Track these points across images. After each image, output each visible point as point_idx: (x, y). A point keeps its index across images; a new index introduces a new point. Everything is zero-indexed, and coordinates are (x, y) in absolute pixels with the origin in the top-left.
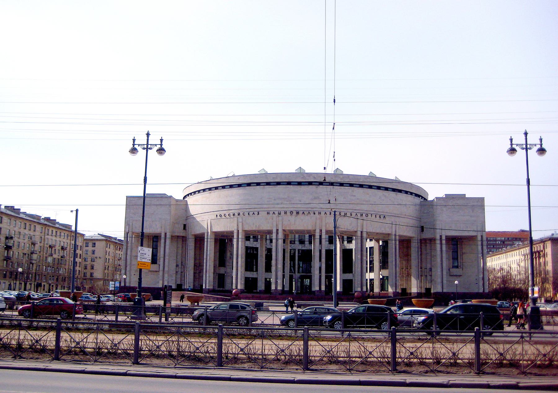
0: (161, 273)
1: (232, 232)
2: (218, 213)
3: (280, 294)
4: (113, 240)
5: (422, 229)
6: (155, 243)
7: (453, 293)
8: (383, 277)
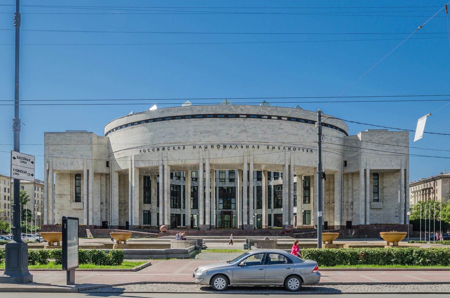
0: (85, 211)
3: (208, 230)
4: (41, 183)
5: (345, 164)
6: (77, 181)
8: (305, 211)
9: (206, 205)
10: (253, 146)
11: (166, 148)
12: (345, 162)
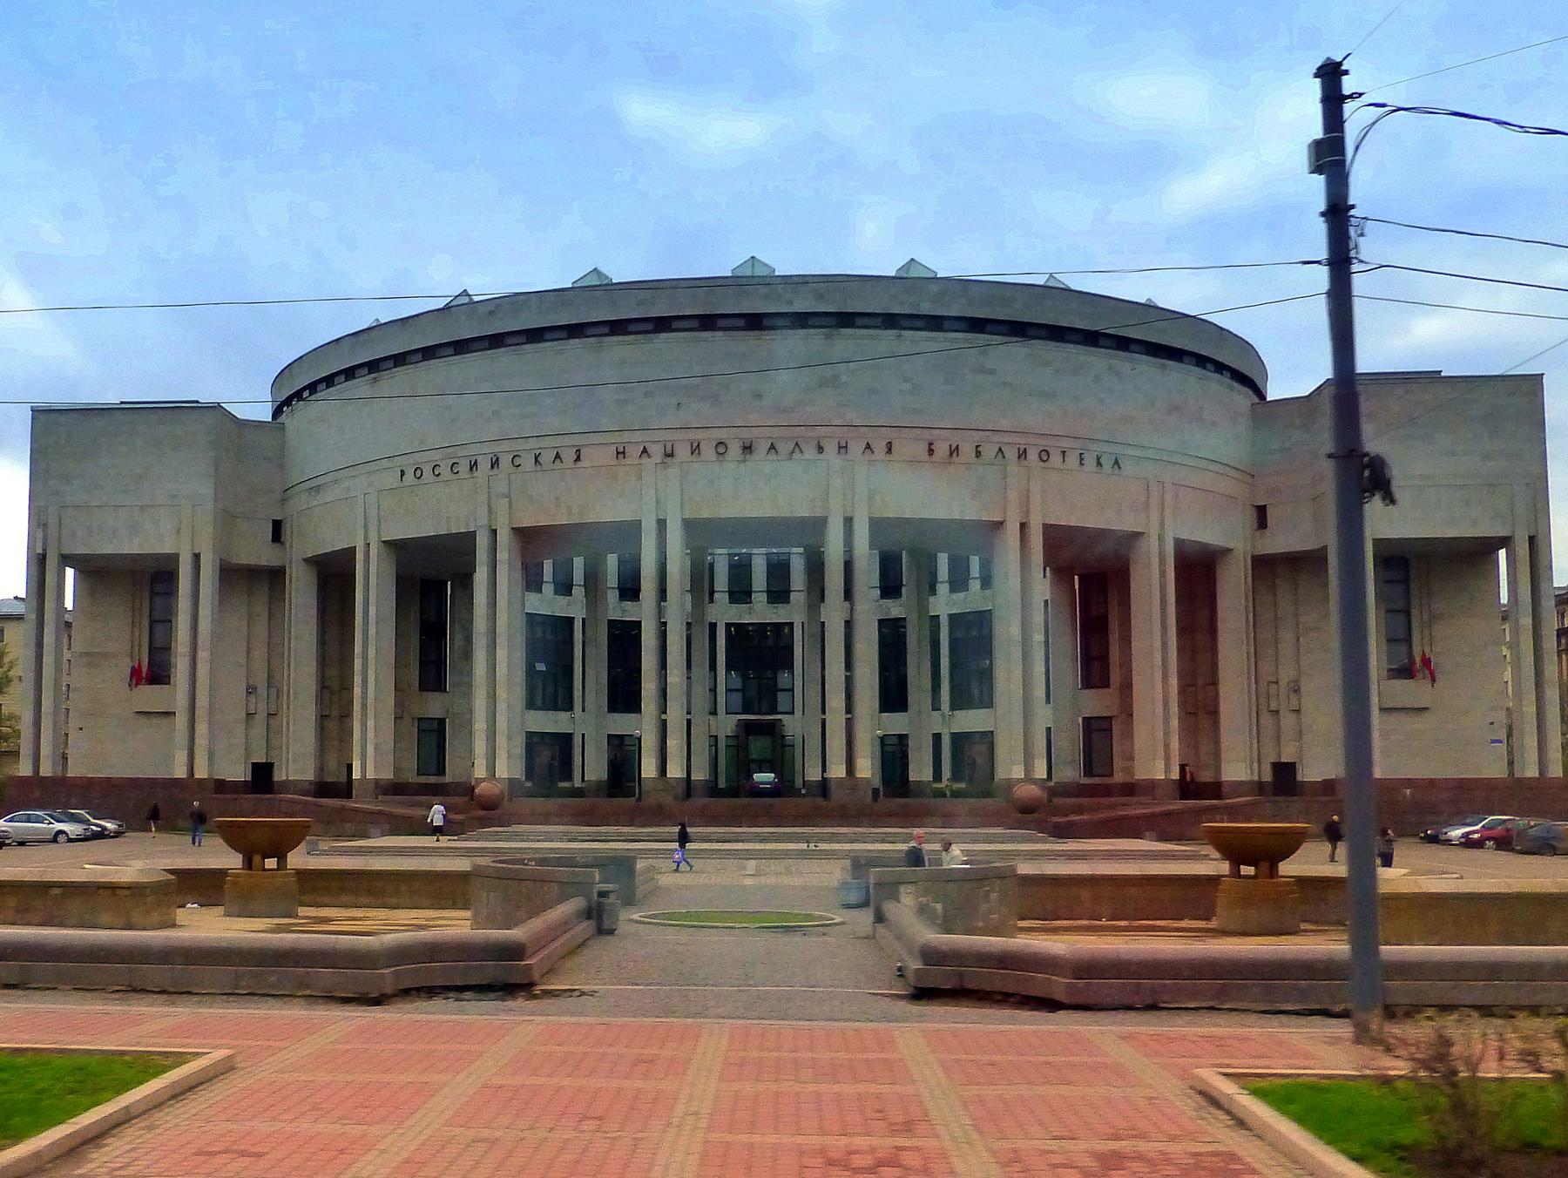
1: (470, 537)
2: (408, 464)
6: (158, 600)
7: (1410, 782)
9: (198, 704)
10: (868, 446)
11: (505, 461)
12: (1261, 511)
